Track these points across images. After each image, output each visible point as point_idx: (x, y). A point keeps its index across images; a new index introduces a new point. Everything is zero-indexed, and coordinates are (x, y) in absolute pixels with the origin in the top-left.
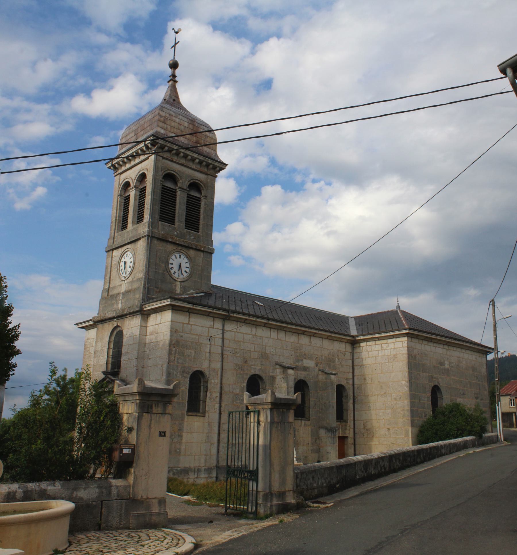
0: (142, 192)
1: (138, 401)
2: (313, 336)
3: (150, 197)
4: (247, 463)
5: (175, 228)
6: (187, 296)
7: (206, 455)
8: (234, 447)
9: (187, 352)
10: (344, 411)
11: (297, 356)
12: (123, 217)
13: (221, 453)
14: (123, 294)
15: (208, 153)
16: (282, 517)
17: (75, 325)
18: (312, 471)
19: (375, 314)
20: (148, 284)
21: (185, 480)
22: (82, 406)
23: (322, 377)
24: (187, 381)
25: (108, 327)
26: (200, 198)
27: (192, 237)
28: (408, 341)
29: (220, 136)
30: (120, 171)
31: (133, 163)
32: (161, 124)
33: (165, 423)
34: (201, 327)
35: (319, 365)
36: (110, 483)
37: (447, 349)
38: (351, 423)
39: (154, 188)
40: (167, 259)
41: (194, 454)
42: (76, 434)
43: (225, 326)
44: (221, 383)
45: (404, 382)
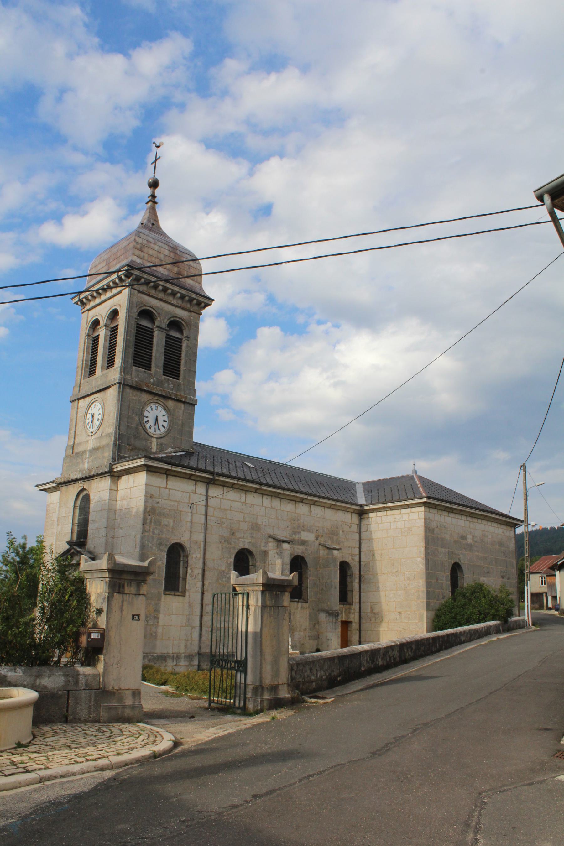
0: (114, 331)
1: (108, 579)
2: (314, 504)
3: (123, 337)
4: (235, 651)
5: (151, 374)
6: (165, 455)
7: (187, 640)
8: (219, 632)
9: (165, 521)
10: (349, 592)
11: (295, 528)
12: (91, 361)
13: (203, 638)
14: (90, 451)
15: (192, 286)
16: (274, 713)
17: (36, 486)
18: (310, 661)
19: (387, 479)
20: (119, 441)
21: (162, 668)
22: (44, 583)
23: (323, 552)
24: (165, 555)
25: (74, 490)
26: (181, 339)
27: (171, 386)
28: (425, 511)
29: (206, 266)
30: (88, 307)
31: (103, 297)
32: (137, 252)
33: (140, 605)
34: (181, 492)
35: (319, 538)
36: (78, 671)
37: (470, 522)
38: (356, 606)
39: (128, 327)
40: (142, 411)
41: (172, 638)
42: (37, 613)
43: (209, 491)
44: (204, 558)
45: (419, 559)
